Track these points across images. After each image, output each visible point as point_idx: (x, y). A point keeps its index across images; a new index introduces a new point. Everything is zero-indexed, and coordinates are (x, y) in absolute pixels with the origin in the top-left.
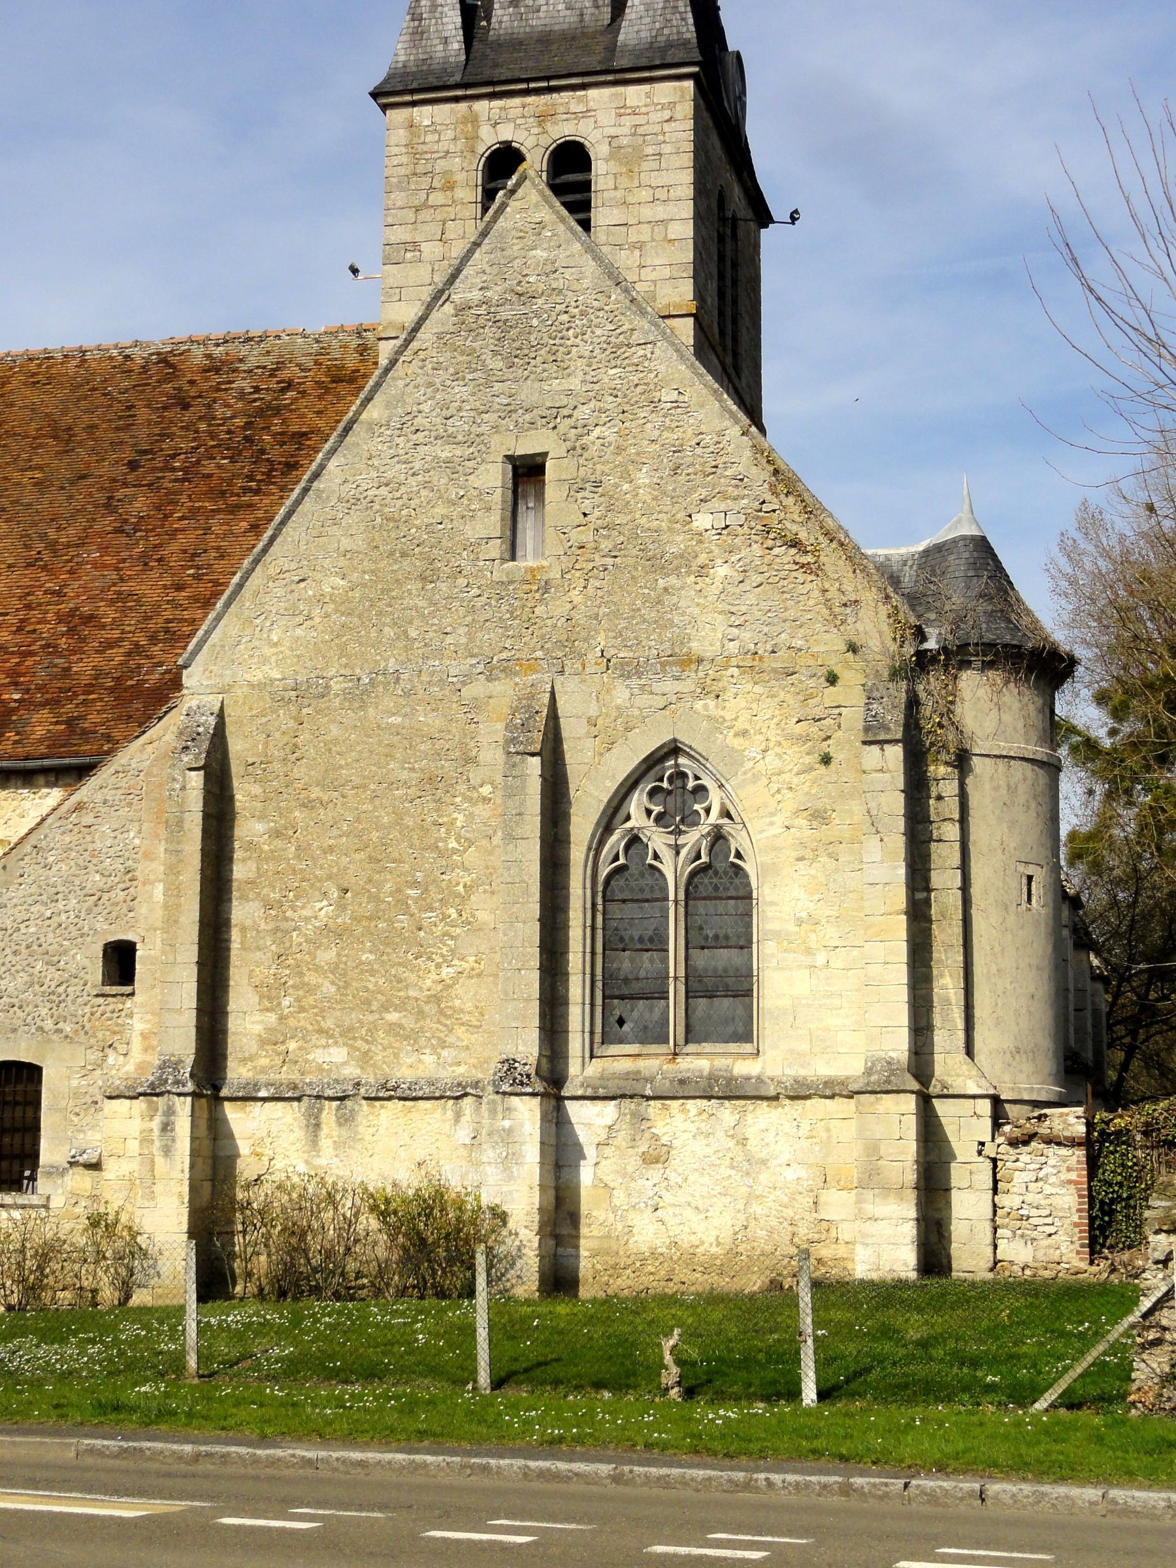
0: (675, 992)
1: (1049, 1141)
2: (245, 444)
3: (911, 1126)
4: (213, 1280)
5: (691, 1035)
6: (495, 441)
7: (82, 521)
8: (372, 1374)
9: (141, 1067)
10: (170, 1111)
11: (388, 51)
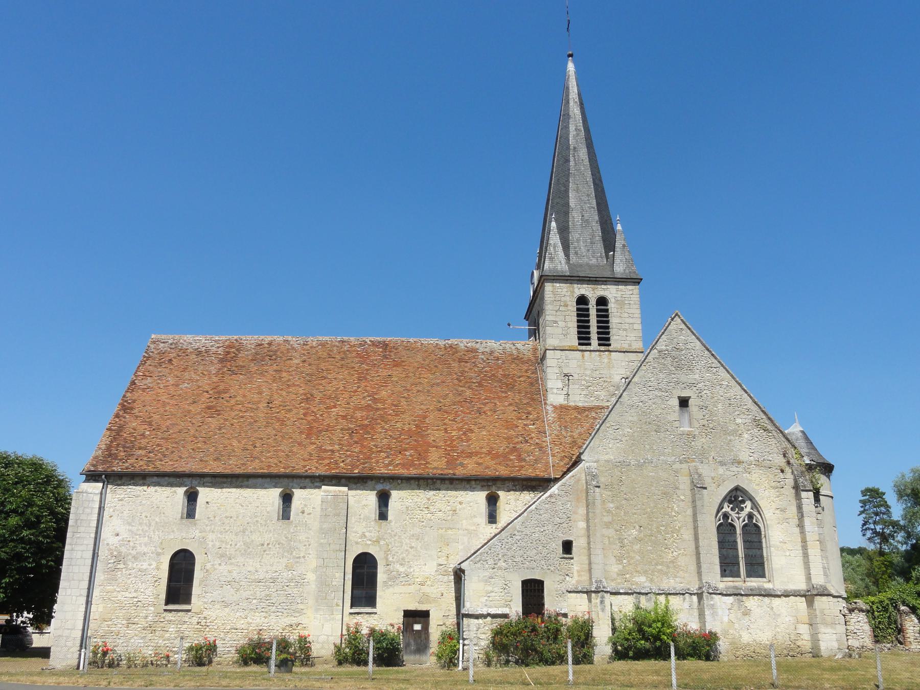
6: (674, 392)
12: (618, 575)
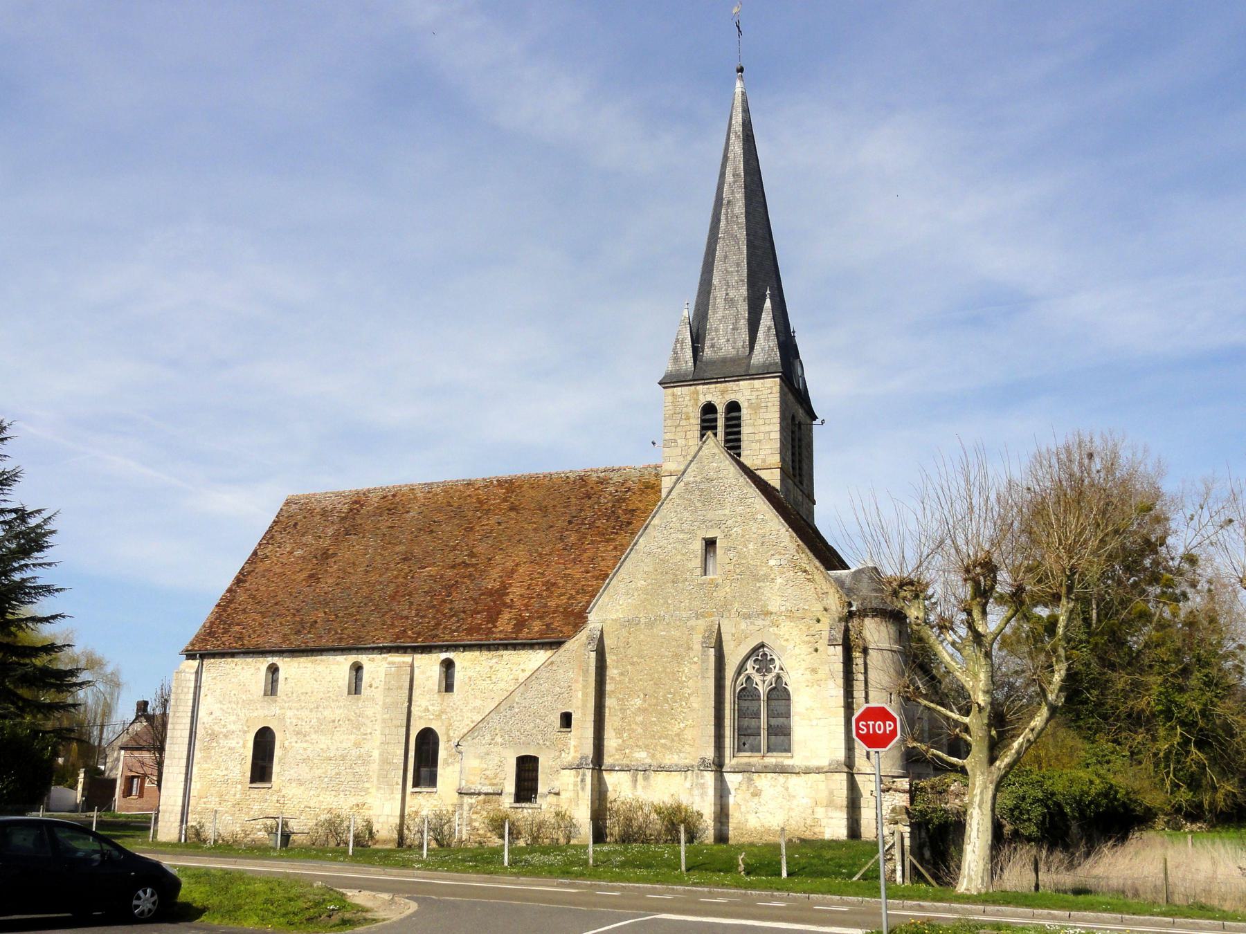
0: (764, 733)
1: (896, 791)
2: (612, 514)
3: (845, 784)
4: (599, 836)
5: (769, 750)
7: (551, 545)
8: (648, 866)
9: (574, 758)
10: (584, 775)
11: (665, 367)
12: (617, 750)
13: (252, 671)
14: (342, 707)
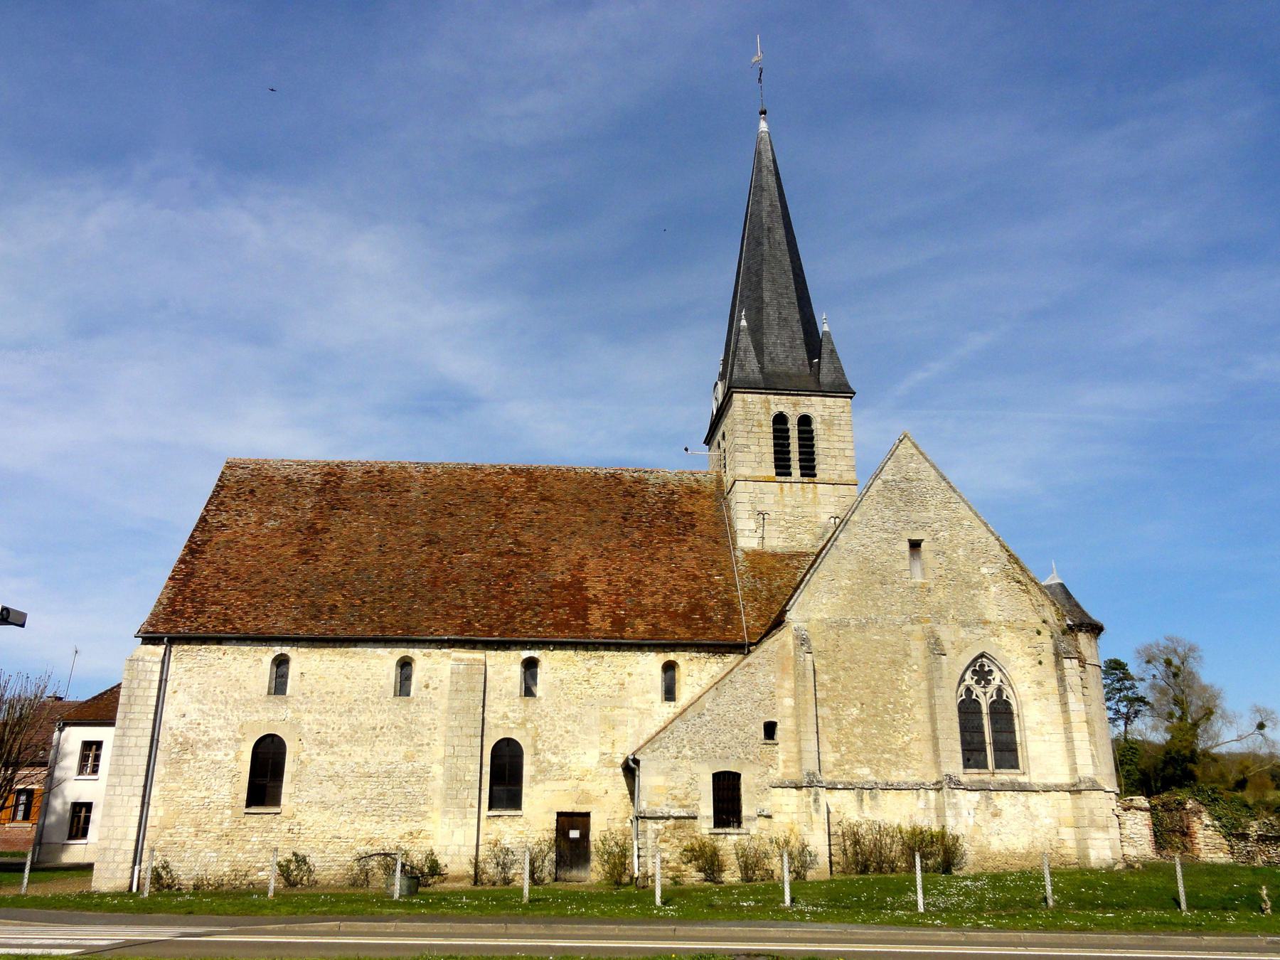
1: (1137, 809)
6: (904, 533)
12: (835, 765)
13: (249, 665)
14: (389, 711)
